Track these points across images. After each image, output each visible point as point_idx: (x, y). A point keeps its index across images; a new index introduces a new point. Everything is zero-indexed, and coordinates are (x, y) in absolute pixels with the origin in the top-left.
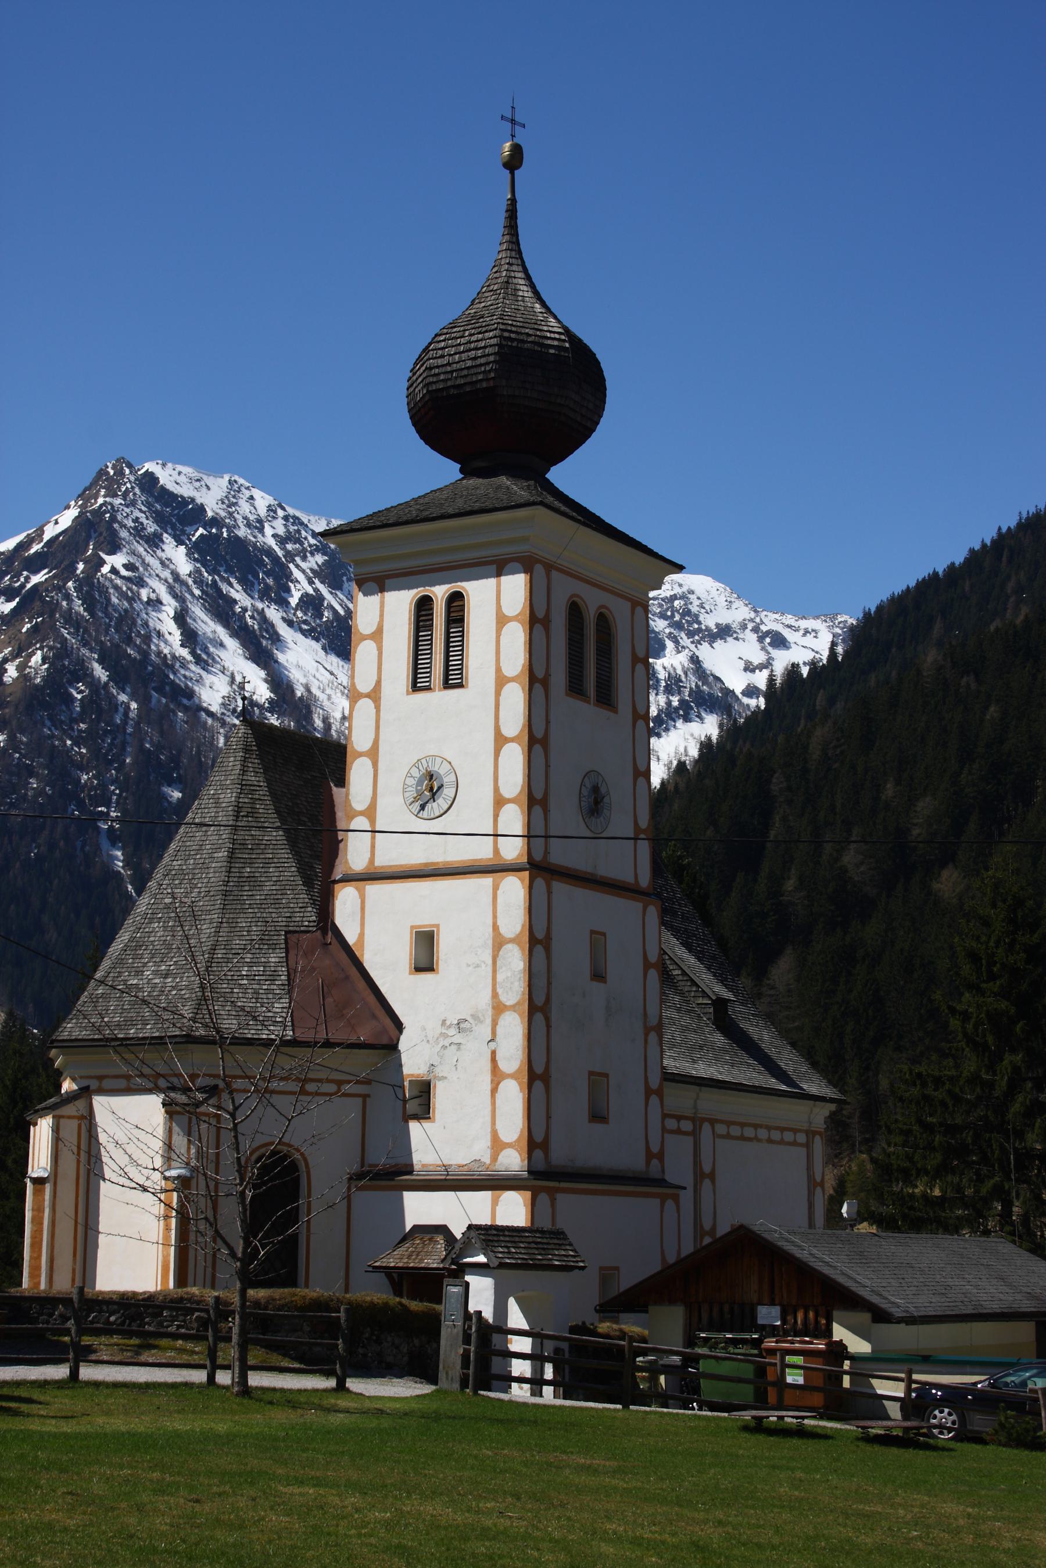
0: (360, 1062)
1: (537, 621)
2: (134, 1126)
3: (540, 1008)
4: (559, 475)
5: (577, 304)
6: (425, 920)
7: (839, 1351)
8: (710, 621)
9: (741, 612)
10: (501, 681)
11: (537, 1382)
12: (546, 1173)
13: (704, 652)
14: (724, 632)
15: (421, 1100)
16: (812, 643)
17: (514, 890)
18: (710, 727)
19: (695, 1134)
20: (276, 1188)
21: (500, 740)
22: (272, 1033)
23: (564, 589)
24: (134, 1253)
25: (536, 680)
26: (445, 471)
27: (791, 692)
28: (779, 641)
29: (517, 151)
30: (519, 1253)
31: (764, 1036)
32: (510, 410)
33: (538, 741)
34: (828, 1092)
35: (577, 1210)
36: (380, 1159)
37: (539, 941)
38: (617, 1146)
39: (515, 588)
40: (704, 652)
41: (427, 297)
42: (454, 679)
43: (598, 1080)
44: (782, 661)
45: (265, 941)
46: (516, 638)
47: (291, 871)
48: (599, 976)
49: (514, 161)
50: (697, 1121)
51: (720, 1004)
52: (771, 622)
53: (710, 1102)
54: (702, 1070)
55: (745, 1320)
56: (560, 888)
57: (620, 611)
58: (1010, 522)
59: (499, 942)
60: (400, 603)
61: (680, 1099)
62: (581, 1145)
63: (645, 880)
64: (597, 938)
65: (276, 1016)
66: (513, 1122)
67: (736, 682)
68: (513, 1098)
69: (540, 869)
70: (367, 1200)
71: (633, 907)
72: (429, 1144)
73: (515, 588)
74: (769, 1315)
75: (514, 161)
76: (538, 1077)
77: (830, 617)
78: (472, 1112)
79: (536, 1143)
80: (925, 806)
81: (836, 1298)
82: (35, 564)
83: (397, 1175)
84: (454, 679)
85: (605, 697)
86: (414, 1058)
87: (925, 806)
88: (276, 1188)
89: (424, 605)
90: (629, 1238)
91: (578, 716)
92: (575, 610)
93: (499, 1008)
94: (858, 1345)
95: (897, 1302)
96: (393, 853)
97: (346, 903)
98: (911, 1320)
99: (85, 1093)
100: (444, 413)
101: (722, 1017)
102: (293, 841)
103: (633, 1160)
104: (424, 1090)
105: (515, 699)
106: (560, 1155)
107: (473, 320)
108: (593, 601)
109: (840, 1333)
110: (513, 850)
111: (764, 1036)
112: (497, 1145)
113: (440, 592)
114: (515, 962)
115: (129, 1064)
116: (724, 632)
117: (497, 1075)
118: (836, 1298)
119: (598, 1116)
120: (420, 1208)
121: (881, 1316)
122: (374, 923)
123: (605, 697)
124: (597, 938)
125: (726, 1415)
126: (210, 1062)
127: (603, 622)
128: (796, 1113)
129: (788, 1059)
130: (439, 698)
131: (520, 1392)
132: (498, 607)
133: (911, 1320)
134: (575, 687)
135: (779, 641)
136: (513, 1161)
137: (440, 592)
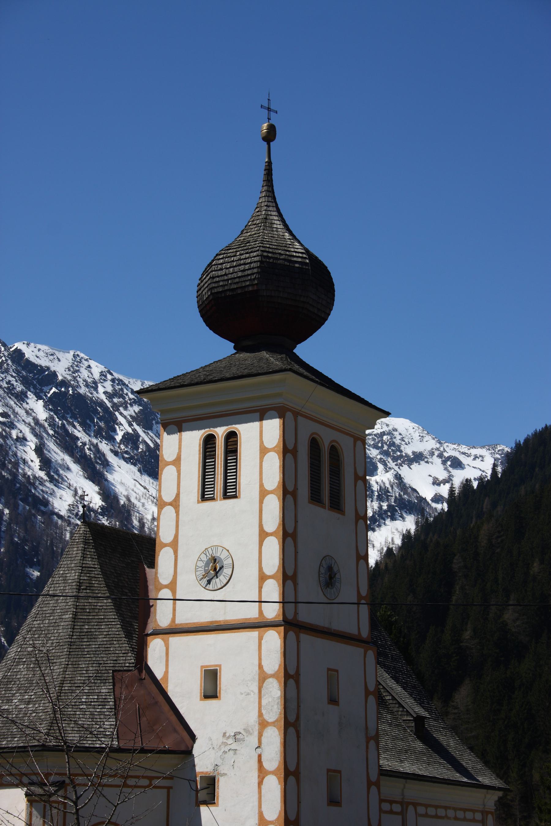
0: (166, 763)
1: (288, 451)
3: (293, 723)
5: (314, 233)
6: (211, 662)
8: (408, 450)
9: (429, 444)
10: (263, 493)
13: (405, 471)
14: (418, 457)
16: (480, 465)
17: (274, 640)
18: (409, 524)
19: (403, 813)
21: (263, 535)
23: (307, 429)
25: (288, 492)
26: (224, 348)
27: (466, 499)
28: (457, 464)
29: (272, 129)
31: (450, 742)
32: (268, 304)
33: (289, 535)
37: (291, 676)
40: (405, 471)
41: (212, 228)
42: (230, 492)
43: (333, 775)
45: (99, 678)
47: (116, 628)
48: (333, 701)
49: (270, 136)
50: (405, 804)
51: (419, 720)
52: (451, 450)
53: (414, 791)
54: (407, 767)
56: (305, 638)
57: (345, 444)
59: (263, 677)
60: (193, 439)
63: (365, 632)
64: (332, 674)
67: (427, 492)
68: (274, 788)
69: (292, 625)
73: (272, 429)
75: (270, 136)
84: (230, 492)
85: (336, 504)
86: (204, 760)
91: (311, 513)
93: (263, 724)
97: (155, 649)
100: (222, 308)
102: (118, 607)
104: (211, 783)
105: (273, 506)
107: (242, 244)
108: (327, 437)
110: (272, 612)
111: (450, 742)
113: (220, 432)
114: (274, 691)
116: (418, 457)
117: (262, 772)
122: (176, 665)
123: (336, 504)
124: (332, 674)
126: (60, 764)
127: (334, 451)
129: (468, 760)
130: (220, 506)
132: (260, 441)
134: (315, 497)
135: (457, 464)
137: (220, 432)
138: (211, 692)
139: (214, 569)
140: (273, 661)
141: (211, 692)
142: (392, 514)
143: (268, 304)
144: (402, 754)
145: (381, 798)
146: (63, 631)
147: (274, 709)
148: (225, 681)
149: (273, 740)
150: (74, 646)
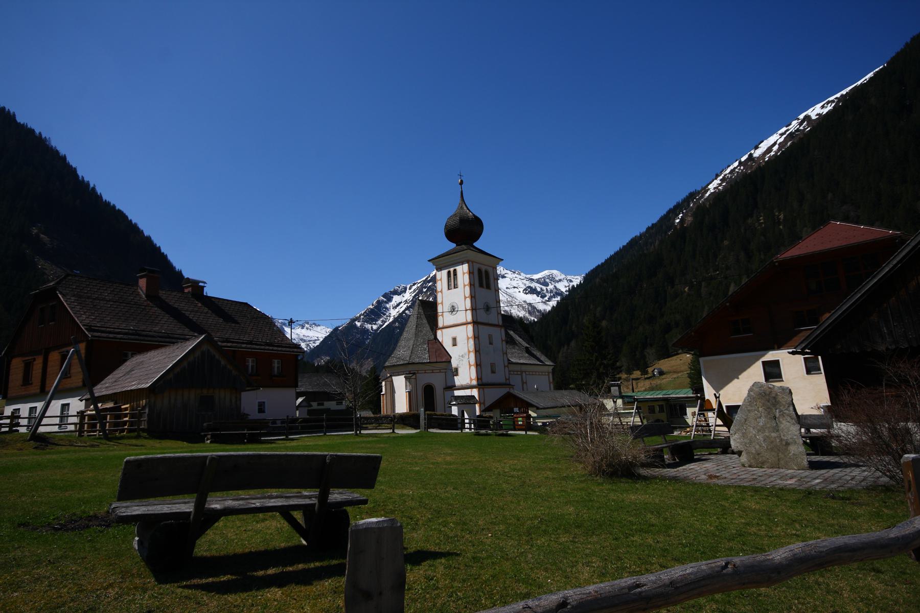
0: (443, 365)
1: (471, 273)
2: (400, 382)
3: (478, 351)
4: (476, 244)
5: (476, 209)
6: (454, 336)
7: (530, 416)
8: (557, 279)
9: (563, 276)
10: (465, 286)
11: (470, 429)
12: (481, 385)
13: (557, 285)
14: (560, 280)
15: (456, 372)
16: (577, 280)
17: (470, 327)
18: (559, 298)
19: (521, 375)
20: (429, 391)
21: (465, 298)
22: (425, 361)
23: (476, 266)
24: (402, 406)
25: (472, 285)
26: (453, 245)
27: (573, 290)
28: (571, 281)
29: (462, 181)
30: (463, 401)
31: (538, 354)
32: (465, 231)
33: (473, 297)
34: (551, 364)
35: (488, 391)
36: (449, 384)
37: (476, 337)
38: (499, 377)
39: (466, 266)
40: (557, 285)
41: (447, 210)
42: (456, 287)
43: (492, 365)
44: (571, 284)
45: (424, 343)
46: (467, 277)
47: (428, 328)
48: (491, 343)
49: (461, 183)
50: (522, 372)
51: (527, 348)
52: (569, 277)
53: (524, 368)
54: (522, 361)
55: (512, 411)
56: (481, 327)
57: (490, 270)
58: (612, 253)
59: (468, 338)
60: (445, 272)
61: (512, 367)
62: (489, 378)
63: (501, 323)
64: (490, 337)
65: (426, 358)
66: (474, 375)
67: (563, 290)
68: (473, 369)
69: (475, 323)
70: (448, 393)
71: (498, 329)
72: (459, 381)
73: (465, 267)
74: (516, 410)
75: (461, 183)
76: (478, 365)
77: (580, 275)
78: (466, 374)
79: (479, 378)
80: (599, 309)
81: (528, 405)
82: (429, 282)
83: (453, 387)
84: (456, 287)
85: (488, 287)
86: (454, 363)
87: (599, 309)
88: (429, 391)
89: (449, 273)
90: (495, 394)
91: (483, 292)
92: (480, 271)
93: (469, 352)
94: (533, 414)
95: (542, 405)
96: (447, 324)
97: (439, 333)
98: (544, 408)
99: (391, 376)
100: (452, 233)
101: (528, 351)
102: (429, 322)
103: (503, 380)
104: (457, 370)
105: (468, 289)
106: (485, 380)
107: (455, 215)
108: (484, 268)
109: (530, 412)
110: (470, 319)
111: (538, 354)
112: (471, 380)
113: (452, 270)
114: (472, 342)
115: (397, 370)
116: (560, 280)
117: (470, 365)
118: (528, 405)
119: (493, 372)
120: (457, 393)
121: (538, 408)
122: (444, 337)
123: (488, 287)
124: (490, 337)
125: (524, 433)
126: (411, 368)
127: (487, 273)
128: (545, 368)
129: (543, 358)
130: (454, 290)
131: (467, 430)
132: (463, 270)
133: (544, 408)
134: (481, 285)
135: (571, 281)
136: (474, 383)
137: (452, 270)
138: (455, 344)
139: (453, 310)
140: (471, 334)
141: (455, 344)
142: (554, 296)
143: (465, 231)
144: (520, 358)
145: (81, 384)
146: (413, 331)
147: (472, 348)
148: (458, 340)
149: (472, 355)
150: (416, 335)
